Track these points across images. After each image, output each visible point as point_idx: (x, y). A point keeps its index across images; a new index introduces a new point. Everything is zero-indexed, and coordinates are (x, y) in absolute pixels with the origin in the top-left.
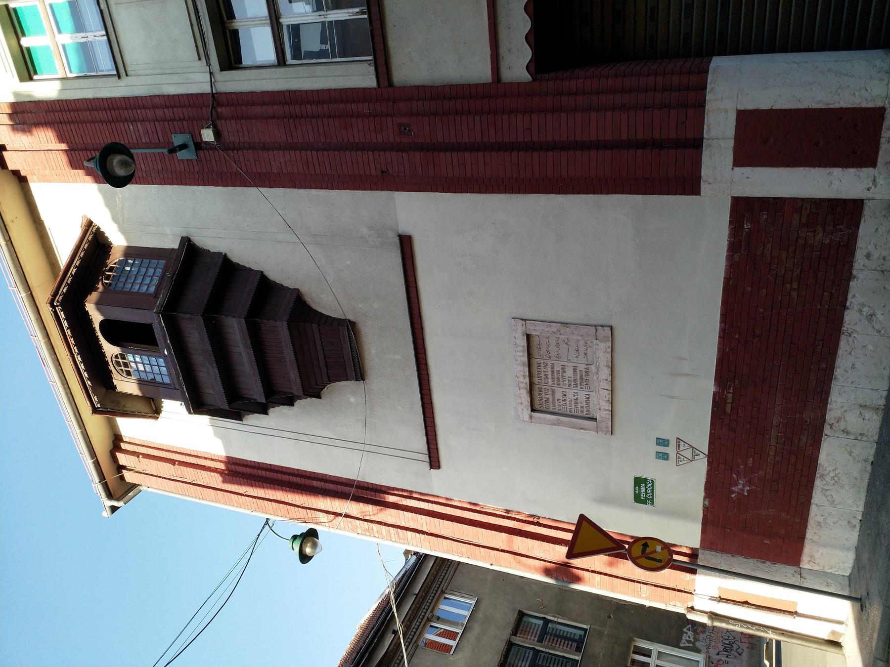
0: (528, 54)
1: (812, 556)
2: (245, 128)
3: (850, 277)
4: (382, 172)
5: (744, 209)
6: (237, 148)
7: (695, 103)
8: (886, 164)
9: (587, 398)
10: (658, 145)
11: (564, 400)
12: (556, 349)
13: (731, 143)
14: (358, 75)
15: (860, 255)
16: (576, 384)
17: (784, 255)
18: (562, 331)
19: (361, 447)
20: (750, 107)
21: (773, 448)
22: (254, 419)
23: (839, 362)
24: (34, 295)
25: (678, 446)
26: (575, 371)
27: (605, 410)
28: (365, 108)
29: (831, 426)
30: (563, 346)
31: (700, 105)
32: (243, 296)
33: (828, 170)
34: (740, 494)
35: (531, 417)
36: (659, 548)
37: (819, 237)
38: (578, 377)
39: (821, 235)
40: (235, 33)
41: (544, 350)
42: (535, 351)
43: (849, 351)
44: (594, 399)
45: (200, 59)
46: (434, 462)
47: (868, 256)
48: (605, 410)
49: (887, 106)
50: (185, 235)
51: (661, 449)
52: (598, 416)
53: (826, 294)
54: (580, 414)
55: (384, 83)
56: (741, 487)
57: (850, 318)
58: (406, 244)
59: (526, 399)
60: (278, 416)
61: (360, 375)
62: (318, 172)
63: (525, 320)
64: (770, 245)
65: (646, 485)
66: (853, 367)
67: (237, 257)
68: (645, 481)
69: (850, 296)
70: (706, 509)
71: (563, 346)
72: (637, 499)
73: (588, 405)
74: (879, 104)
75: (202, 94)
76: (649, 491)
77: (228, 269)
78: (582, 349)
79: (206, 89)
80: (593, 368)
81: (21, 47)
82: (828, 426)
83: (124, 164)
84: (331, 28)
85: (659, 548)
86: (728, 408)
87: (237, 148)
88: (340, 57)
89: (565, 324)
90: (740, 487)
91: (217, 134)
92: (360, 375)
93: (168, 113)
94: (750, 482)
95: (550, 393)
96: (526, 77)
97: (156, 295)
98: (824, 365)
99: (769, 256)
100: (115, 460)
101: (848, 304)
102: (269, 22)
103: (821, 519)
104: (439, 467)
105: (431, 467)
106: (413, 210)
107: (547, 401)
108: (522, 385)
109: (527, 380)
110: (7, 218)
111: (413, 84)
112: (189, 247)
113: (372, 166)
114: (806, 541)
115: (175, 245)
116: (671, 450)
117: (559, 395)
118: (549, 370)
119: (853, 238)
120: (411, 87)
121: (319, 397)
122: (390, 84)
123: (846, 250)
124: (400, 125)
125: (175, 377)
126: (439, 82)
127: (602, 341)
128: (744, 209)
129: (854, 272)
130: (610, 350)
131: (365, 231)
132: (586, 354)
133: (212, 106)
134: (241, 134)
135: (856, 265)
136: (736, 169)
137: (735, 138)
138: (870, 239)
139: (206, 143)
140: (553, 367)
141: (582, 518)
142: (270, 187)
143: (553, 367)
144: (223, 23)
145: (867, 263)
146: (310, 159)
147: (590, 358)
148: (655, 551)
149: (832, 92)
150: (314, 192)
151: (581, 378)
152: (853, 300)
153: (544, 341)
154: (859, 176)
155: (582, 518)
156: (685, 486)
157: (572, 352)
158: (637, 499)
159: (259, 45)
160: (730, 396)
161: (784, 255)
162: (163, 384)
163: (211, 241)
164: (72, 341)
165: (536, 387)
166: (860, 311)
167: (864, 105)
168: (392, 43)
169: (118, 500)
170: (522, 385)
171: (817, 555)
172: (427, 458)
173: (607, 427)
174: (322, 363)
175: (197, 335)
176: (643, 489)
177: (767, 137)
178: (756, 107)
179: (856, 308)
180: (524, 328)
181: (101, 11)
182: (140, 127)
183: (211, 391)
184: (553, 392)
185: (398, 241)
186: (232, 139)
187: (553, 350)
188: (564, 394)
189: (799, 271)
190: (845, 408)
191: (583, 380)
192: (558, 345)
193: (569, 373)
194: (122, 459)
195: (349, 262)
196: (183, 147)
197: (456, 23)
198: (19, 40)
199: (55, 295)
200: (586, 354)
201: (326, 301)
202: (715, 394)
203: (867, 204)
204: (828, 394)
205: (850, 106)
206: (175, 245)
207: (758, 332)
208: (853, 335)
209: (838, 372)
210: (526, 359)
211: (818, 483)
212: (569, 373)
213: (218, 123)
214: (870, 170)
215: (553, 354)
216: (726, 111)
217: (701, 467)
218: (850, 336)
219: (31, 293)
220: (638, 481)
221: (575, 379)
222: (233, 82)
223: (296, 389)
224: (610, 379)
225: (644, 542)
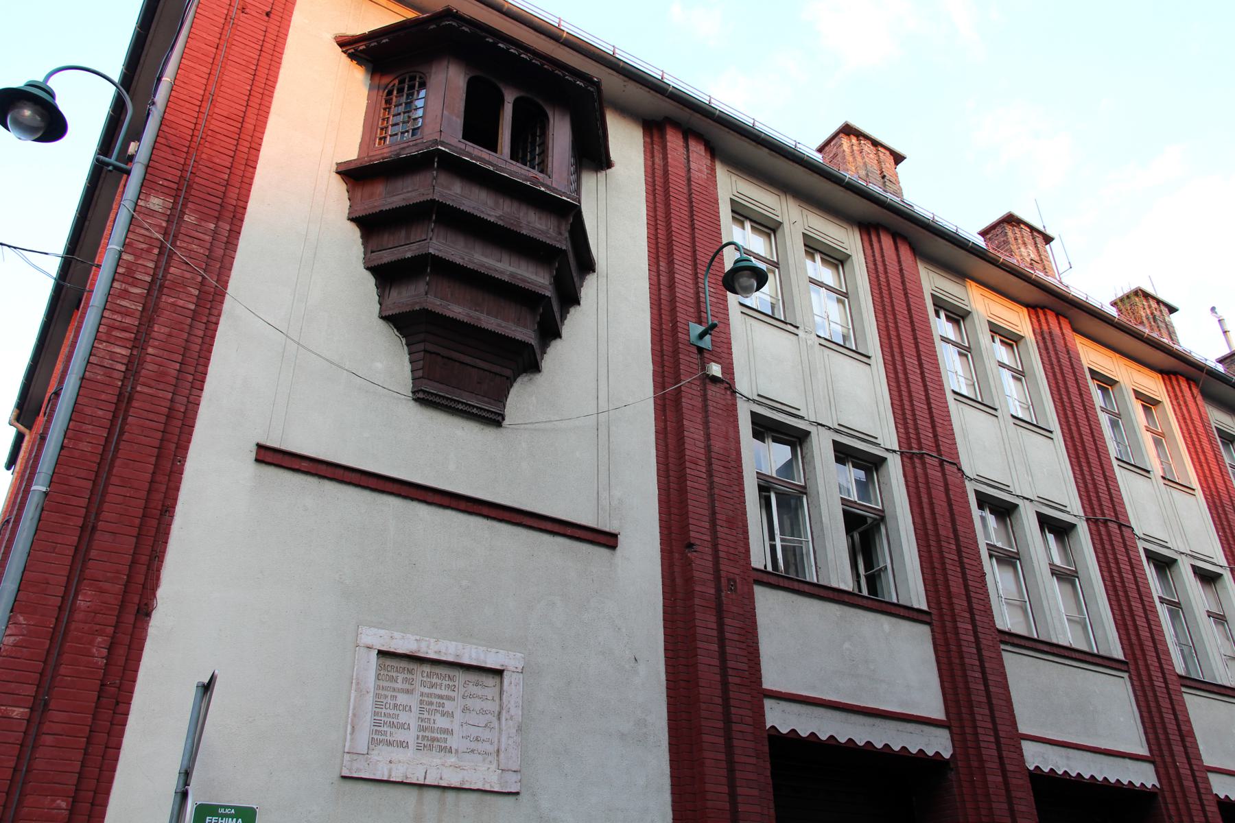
0: (784, 730)
9: (403, 745)
12: (478, 708)
16: (424, 729)
38: (435, 735)
41: (473, 689)
42: (473, 677)
44: (397, 754)
73: (390, 744)
78: (480, 747)
80: (452, 759)
95: (407, 686)
109: (432, 656)
117: (402, 699)
118: (444, 692)
127: (500, 778)
130: (488, 788)
132: (473, 751)
151: (433, 739)
157: (475, 732)
191: (431, 742)
193: (442, 722)
200: (473, 751)
201: (523, 399)
210: (466, 661)
212: (442, 722)
224: (443, 783)
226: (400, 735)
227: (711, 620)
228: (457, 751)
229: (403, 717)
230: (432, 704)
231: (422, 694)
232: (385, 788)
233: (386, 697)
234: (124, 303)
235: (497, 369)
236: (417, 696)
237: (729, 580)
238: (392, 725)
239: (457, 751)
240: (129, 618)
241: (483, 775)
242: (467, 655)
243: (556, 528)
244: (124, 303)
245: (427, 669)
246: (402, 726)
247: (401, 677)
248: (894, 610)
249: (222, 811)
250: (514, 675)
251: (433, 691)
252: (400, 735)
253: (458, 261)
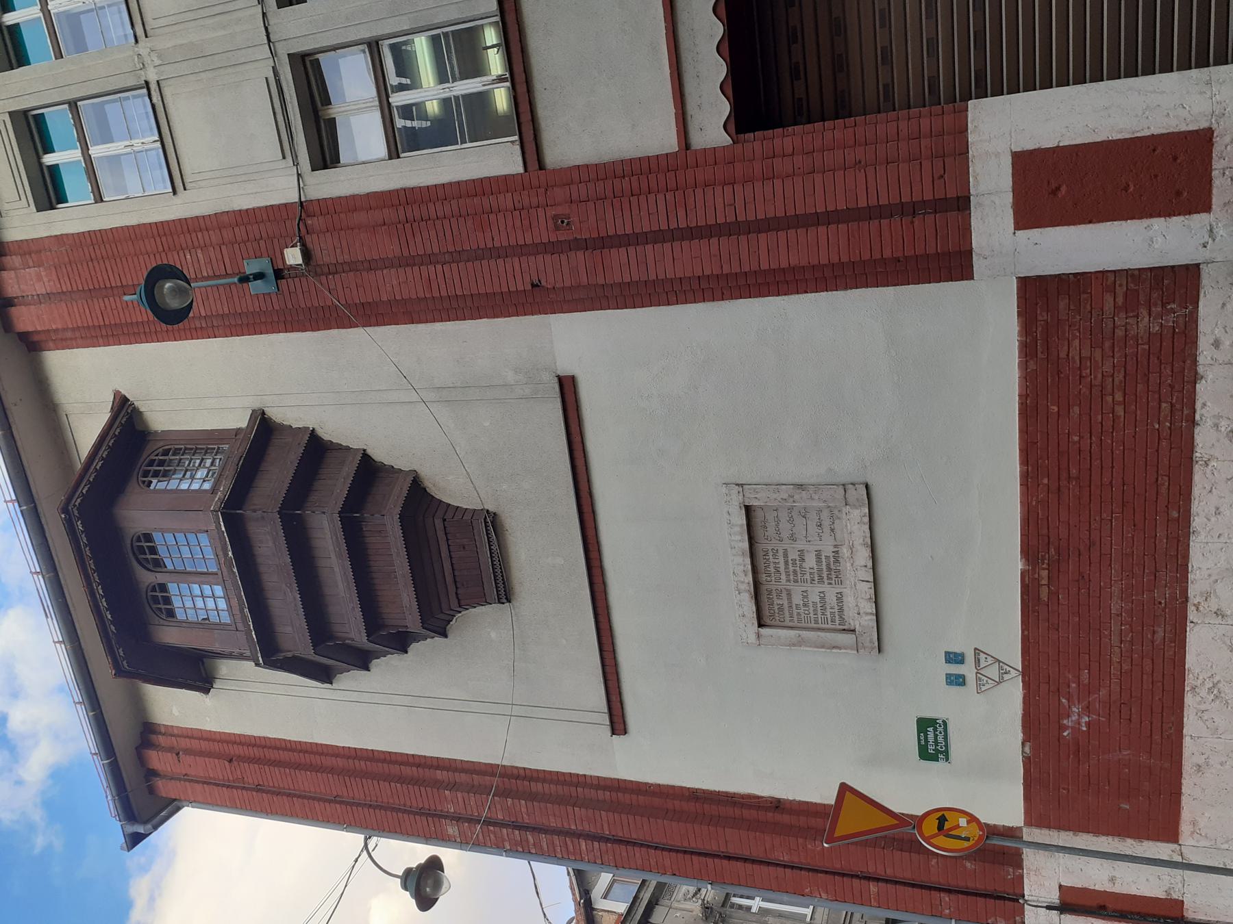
0: (725, 108)
1: (1194, 823)
2: (344, 244)
3: (1195, 378)
4: (533, 286)
5: (1041, 297)
6: (334, 270)
7: (954, 150)
8: (1225, 204)
9: (840, 598)
10: (910, 210)
11: (805, 605)
12: (789, 526)
13: (1009, 198)
14: (498, 158)
15: (1204, 343)
16: (821, 580)
17: (1098, 354)
18: (797, 497)
19: (507, 710)
20: (1030, 145)
21: (1117, 650)
22: (351, 681)
23: (1195, 507)
24: (40, 509)
25: (977, 661)
26: (818, 557)
27: (867, 614)
28: (506, 200)
29: (1197, 607)
30: (799, 521)
31: (962, 152)
32: (336, 485)
33: (1146, 222)
34: (1076, 730)
35: (759, 636)
36: (963, 822)
37: (1145, 324)
38: (824, 567)
39: (1146, 319)
40: (332, 123)
41: (771, 531)
42: (759, 533)
43: (1208, 488)
44: (849, 601)
45: (284, 158)
46: (618, 724)
47: (1217, 344)
48: (867, 614)
49: (1214, 126)
50: (257, 405)
51: (955, 669)
52: (855, 623)
53: (1164, 405)
54: (830, 626)
55: (533, 165)
56: (1077, 719)
57: (1204, 439)
58: (567, 388)
59: (750, 608)
60: (390, 671)
61: (505, 594)
62: (444, 293)
63: (742, 485)
64: (1077, 341)
65: (935, 730)
66: (1218, 512)
67: (328, 433)
68: (932, 722)
69: (1198, 405)
70: (1027, 762)
71: (799, 521)
72: (924, 754)
73: (841, 610)
74: (1204, 125)
75: (286, 205)
76: (940, 738)
77: (317, 450)
78: (826, 523)
79: (293, 197)
80: (845, 551)
81: (41, 164)
82: (1193, 608)
83: (178, 291)
84: (458, 106)
85: (963, 822)
86: (1044, 593)
87: (334, 270)
88: (471, 141)
89: (800, 486)
90: (1075, 718)
91: (306, 254)
92: (505, 594)
93: (240, 232)
94: (1088, 709)
95: (784, 595)
96: (726, 140)
97: (214, 491)
98: (1175, 514)
99: (1077, 358)
100: (141, 760)
101: (1197, 417)
102: (377, 103)
103: (1201, 760)
104: (625, 732)
105: (613, 733)
106: (578, 340)
107: (781, 609)
108: (743, 587)
109: (750, 578)
110: (9, 400)
111: (572, 164)
112: (264, 429)
113: (519, 277)
114: (1184, 799)
115: (243, 423)
116: (968, 670)
117: (797, 599)
118: (782, 560)
119: (1192, 321)
120: (571, 169)
121: (444, 634)
122: (541, 167)
123: (1183, 339)
124: (555, 217)
125: (236, 611)
126: (606, 159)
127: (855, 507)
128: (1041, 297)
129: (1200, 370)
130: (866, 519)
131: (510, 377)
132: (832, 530)
133: (302, 218)
134: (338, 251)
135: (1201, 359)
136: (1018, 233)
137: (1013, 191)
138: (1216, 316)
139: (291, 267)
140: (786, 555)
141: (844, 789)
142: (378, 325)
143: (786, 555)
144: (316, 112)
145: (1216, 354)
146: (433, 277)
147: (838, 536)
148: (958, 826)
149: (1137, 116)
150: (438, 326)
151: (829, 569)
152: (1204, 411)
153: (771, 517)
154: (1189, 227)
155: (844, 789)
156: (993, 725)
157: (813, 529)
158: (924, 754)
159: (363, 135)
160: (1045, 573)
161: (1098, 354)
162: (220, 624)
163: (292, 412)
164: (91, 564)
165: (763, 589)
166: (1216, 426)
167: (1184, 128)
168: (542, 112)
169: (145, 823)
170: (743, 587)
171: (1202, 823)
172: (606, 719)
173: (871, 641)
174: (449, 579)
175: (271, 544)
176: (931, 736)
177: (1056, 186)
178: (1036, 147)
179: (1209, 423)
180: (741, 497)
181: (153, 106)
182: (200, 255)
183: (289, 629)
184: (789, 595)
185: (557, 387)
186: (327, 260)
187: (785, 526)
188: (805, 595)
189: (1121, 376)
190: (1213, 578)
191: (831, 571)
192: (791, 520)
193: (810, 561)
194: (157, 760)
195: (487, 424)
196: (259, 276)
197: (628, 83)
198: (39, 158)
199: (69, 500)
200: (832, 530)
201: (455, 487)
202: (1023, 574)
203: (1205, 270)
204: (1186, 557)
205: (1164, 131)
206: (243, 423)
207: (1074, 472)
208: (1213, 463)
209: (1197, 523)
210: (746, 545)
211: (1189, 699)
212: (810, 561)
213: (308, 239)
214: (1204, 216)
215: (785, 535)
216: (997, 155)
217: (1014, 692)
218: (1207, 465)
219: (35, 507)
220: (924, 724)
221: (820, 570)
222: (328, 185)
223: (412, 620)
224: (870, 564)
225: (940, 814)
226: (831, 599)
227: (617, 256)
228: (836, 546)
229: (814, 597)
230: (795, 572)
231: (789, 581)
232: (883, 569)
233: (799, 614)
234: (545, 847)
235: (441, 534)
236: (791, 586)
237: (557, 228)
238: (824, 608)
239: (836, 546)
240: (786, 819)
241: (853, 524)
242: (740, 544)
243: (578, 454)
244: (545, 847)
245: (763, 577)
246: (823, 599)
247: (776, 601)
248: (520, 78)
249: (923, 742)
250: (747, 495)
251: (782, 569)
252: (831, 599)
253: (359, 614)
